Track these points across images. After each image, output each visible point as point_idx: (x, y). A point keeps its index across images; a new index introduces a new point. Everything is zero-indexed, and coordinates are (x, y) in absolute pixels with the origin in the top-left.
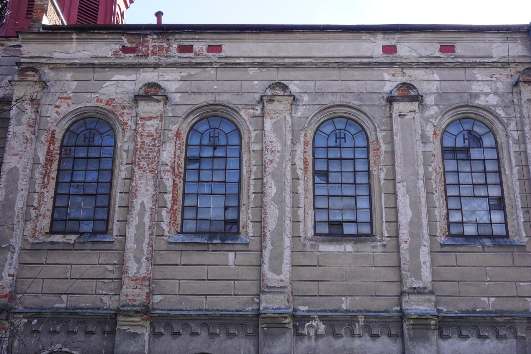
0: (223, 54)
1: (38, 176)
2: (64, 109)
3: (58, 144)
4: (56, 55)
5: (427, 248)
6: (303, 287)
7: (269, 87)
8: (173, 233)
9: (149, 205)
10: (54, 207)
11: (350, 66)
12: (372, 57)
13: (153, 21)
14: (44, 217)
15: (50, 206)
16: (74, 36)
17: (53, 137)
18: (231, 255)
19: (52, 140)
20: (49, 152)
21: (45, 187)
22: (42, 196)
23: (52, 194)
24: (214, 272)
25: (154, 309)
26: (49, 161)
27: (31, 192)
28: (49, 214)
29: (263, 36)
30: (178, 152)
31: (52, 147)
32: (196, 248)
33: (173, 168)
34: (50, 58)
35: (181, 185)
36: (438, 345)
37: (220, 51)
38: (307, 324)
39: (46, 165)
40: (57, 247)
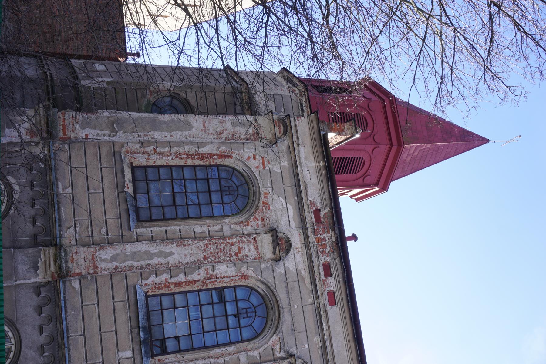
0: (328, 307)
2: (254, 164)
4: (302, 149)
9: (171, 260)
10: (158, 167)
14: (147, 159)
15: (159, 163)
19: (222, 156)
20: (211, 155)
22: (168, 154)
23: (171, 164)
25: (64, 283)
26: (202, 157)
27: (170, 144)
28: (151, 163)
29: (353, 345)
30: (228, 280)
33: (211, 277)
34: (298, 144)
35: (195, 287)
40: (119, 176)
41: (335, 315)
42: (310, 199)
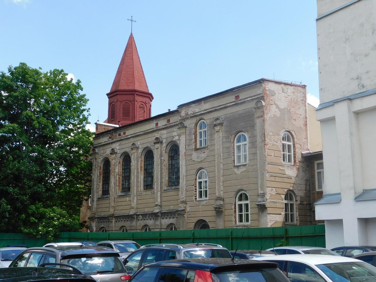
1: (98, 180)
2: (102, 159)
3: (102, 169)
5: (113, 212)
6: (139, 206)
7: (132, 145)
8: (119, 192)
9: (113, 186)
11: (149, 133)
12: (153, 128)
13: (168, 111)
16: (101, 136)
17: (100, 168)
18: (128, 198)
20: (100, 172)
21: (100, 182)
22: (99, 185)
24: (123, 203)
30: (120, 168)
31: (100, 171)
32: (122, 197)
36: (160, 221)
37: (239, 98)
38: (33, 272)
39: (99, 176)
42: (107, 140)
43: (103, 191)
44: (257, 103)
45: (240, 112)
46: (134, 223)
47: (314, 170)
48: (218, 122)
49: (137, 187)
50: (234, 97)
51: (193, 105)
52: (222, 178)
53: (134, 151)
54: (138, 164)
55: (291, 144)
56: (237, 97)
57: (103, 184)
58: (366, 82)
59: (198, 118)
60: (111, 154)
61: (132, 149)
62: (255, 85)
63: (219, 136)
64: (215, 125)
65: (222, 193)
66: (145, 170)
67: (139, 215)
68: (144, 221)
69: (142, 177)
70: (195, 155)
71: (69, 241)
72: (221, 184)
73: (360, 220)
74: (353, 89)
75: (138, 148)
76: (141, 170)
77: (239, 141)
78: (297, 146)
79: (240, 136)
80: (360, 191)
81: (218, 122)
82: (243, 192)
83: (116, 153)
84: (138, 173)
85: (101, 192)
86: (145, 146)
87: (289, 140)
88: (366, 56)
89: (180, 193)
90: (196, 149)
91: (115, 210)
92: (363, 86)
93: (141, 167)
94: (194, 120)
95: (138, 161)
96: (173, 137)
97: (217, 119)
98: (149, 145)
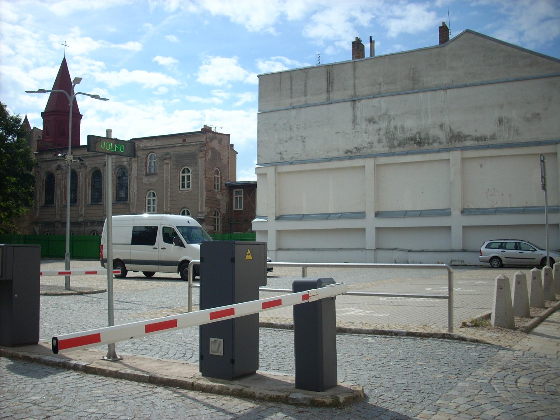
20: (43, 184)
26: (43, 186)
41: (188, 140)
43: (46, 201)
44: (200, 148)
45: (186, 152)
46: (82, 229)
47: (233, 196)
48: (168, 156)
49: (85, 199)
50: (182, 140)
51: (145, 141)
52: (169, 199)
53: (82, 170)
54: (86, 181)
55: (219, 176)
56: (184, 141)
57: (46, 195)
58: (285, 157)
59: (149, 151)
60: (57, 169)
61: (80, 168)
62: (391, 267)
63: (168, 167)
64: (165, 159)
65: (169, 209)
66: (93, 186)
67: (87, 222)
68: (93, 228)
69: (89, 192)
70: (145, 180)
71: (70, 241)
72: (169, 203)
73: (463, 226)
74: (277, 158)
75: (86, 167)
76: (89, 185)
77: (184, 172)
78: (223, 178)
79: (151, 156)
80: (278, 215)
81: (168, 156)
82: (186, 209)
83: (62, 169)
84: (86, 188)
85: (44, 202)
86: (93, 166)
87: (218, 174)
88: (286, 142)
89: (131, 207)
90: (147, 175)
91: (61, 217)
92: (283, 158)
93: (89, 184)
94: (146, 152)
95: (86, 179)
96: (123, 162)
97: (167, 154)
98: (98, 166)
